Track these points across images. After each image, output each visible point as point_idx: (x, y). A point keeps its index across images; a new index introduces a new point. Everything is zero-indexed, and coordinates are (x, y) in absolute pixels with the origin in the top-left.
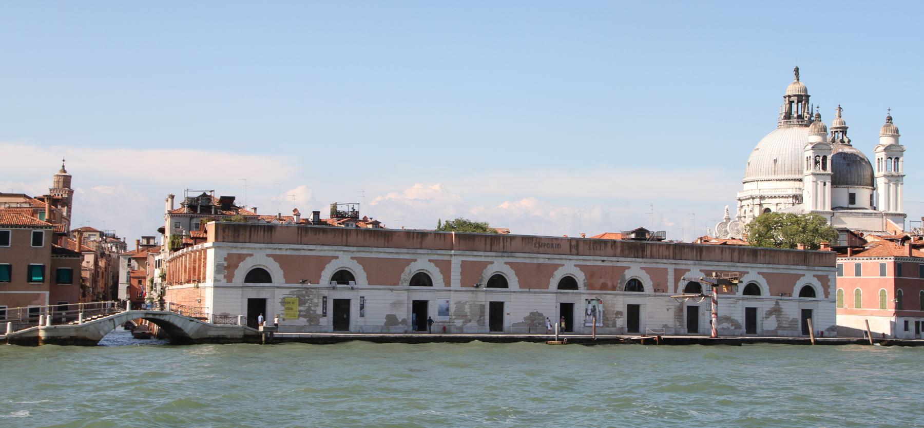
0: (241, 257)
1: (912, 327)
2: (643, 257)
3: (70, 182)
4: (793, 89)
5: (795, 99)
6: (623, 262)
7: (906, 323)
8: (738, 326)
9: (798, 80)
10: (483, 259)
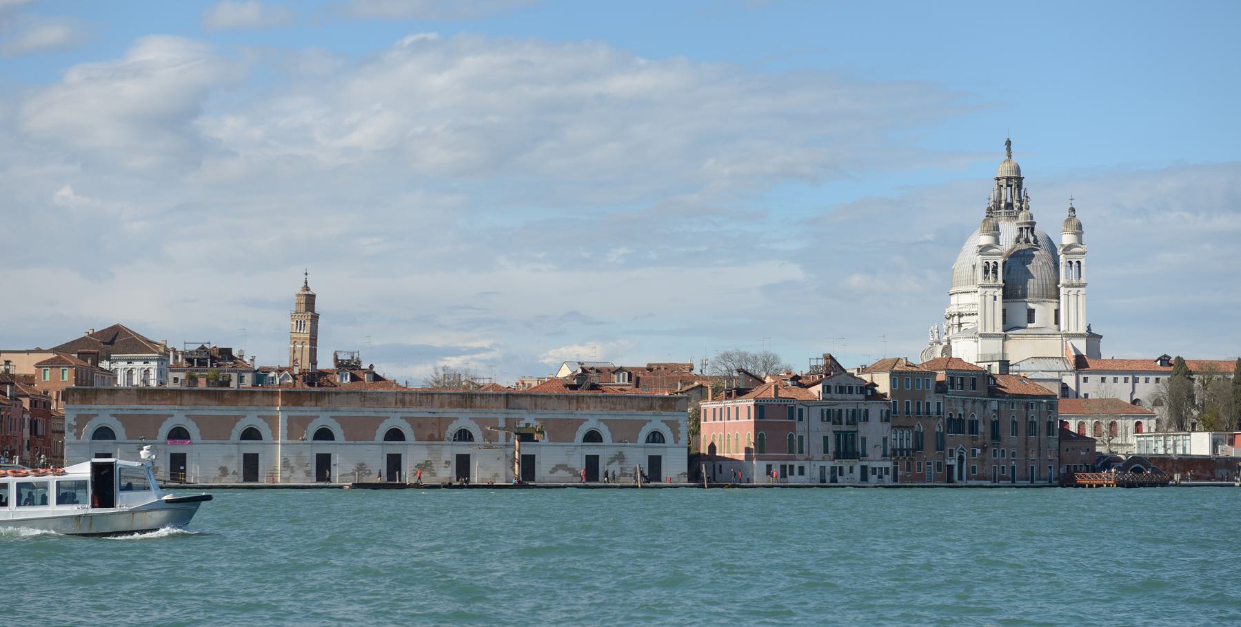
0: (88, 418)
1: (776, 470)
2: (471, 407)
3: (313, 304)
4: (1004, 170)
5: (1003, 182)
6: (449, 412)
7: (769, 467)
8: (576, 474)
9: (1010, 156)
10: (308, 414)
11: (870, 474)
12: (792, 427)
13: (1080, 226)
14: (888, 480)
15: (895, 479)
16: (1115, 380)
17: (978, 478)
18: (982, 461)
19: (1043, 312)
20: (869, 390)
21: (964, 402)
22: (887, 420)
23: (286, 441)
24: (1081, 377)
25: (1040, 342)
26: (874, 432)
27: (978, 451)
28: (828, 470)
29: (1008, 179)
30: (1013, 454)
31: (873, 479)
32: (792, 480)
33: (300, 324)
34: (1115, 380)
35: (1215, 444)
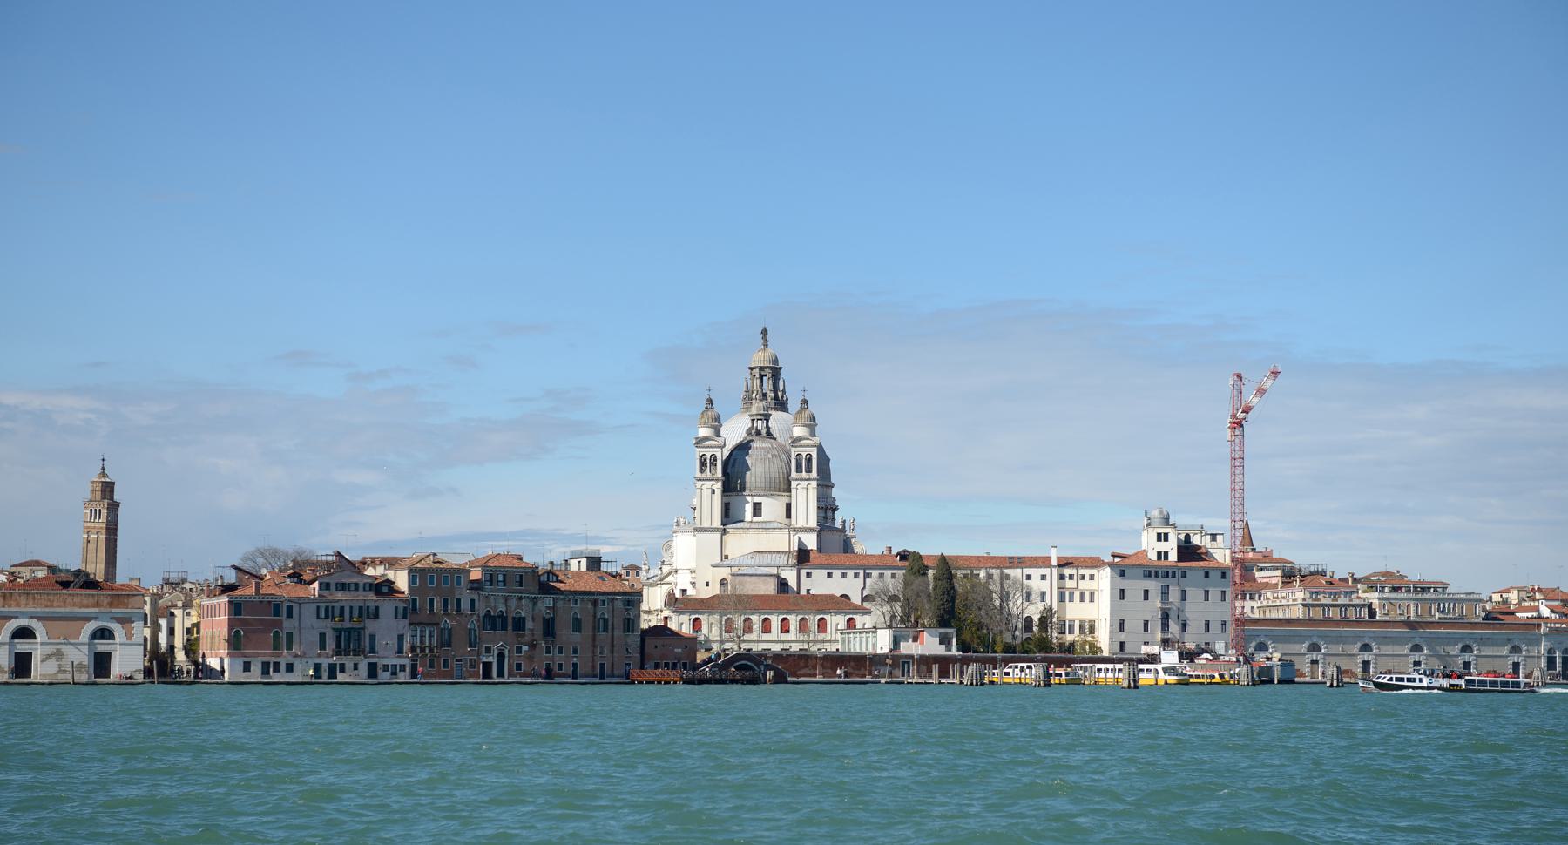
4: (760, 359)
5: (756, 372)
9: (766, 346)
11: (380, 671)
12: (279, 624)
13: (813, 418)
14: (403, 676)
15: (414, 675)
16: (844, 576)
17: (525, 675)
18: (530, 658)
19: (772, 508)
20: (384, 588)
21: (506, 599)
22: (404, 617)
23: (46, 639)
24: (803, 572)
25: (763, 536)
26: (386, 630)
27: (525, 648)
28: (325, 667)
29: (761, 368)
30: (575, 651)
31: (384, 676)
32: (276, 677)
33: (95, 513)
34: (844, 576)
35: (896, 642)
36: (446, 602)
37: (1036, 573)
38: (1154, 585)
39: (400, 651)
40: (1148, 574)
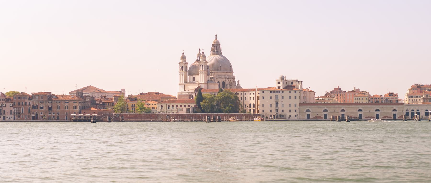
14: (12, 119)
15: (14, 119)
31: (7, 119)
36: (23, 103)
37: (252, 93)
38: (273, 95)
39: (11, 114)
40: (277, 92)
